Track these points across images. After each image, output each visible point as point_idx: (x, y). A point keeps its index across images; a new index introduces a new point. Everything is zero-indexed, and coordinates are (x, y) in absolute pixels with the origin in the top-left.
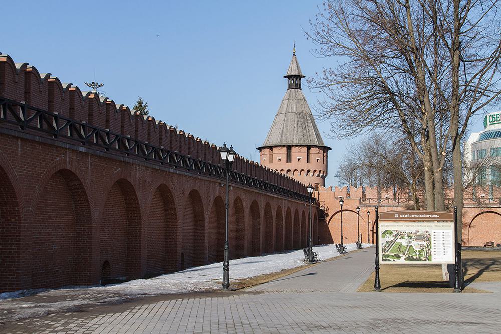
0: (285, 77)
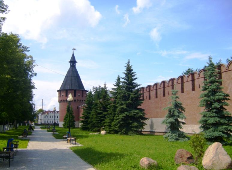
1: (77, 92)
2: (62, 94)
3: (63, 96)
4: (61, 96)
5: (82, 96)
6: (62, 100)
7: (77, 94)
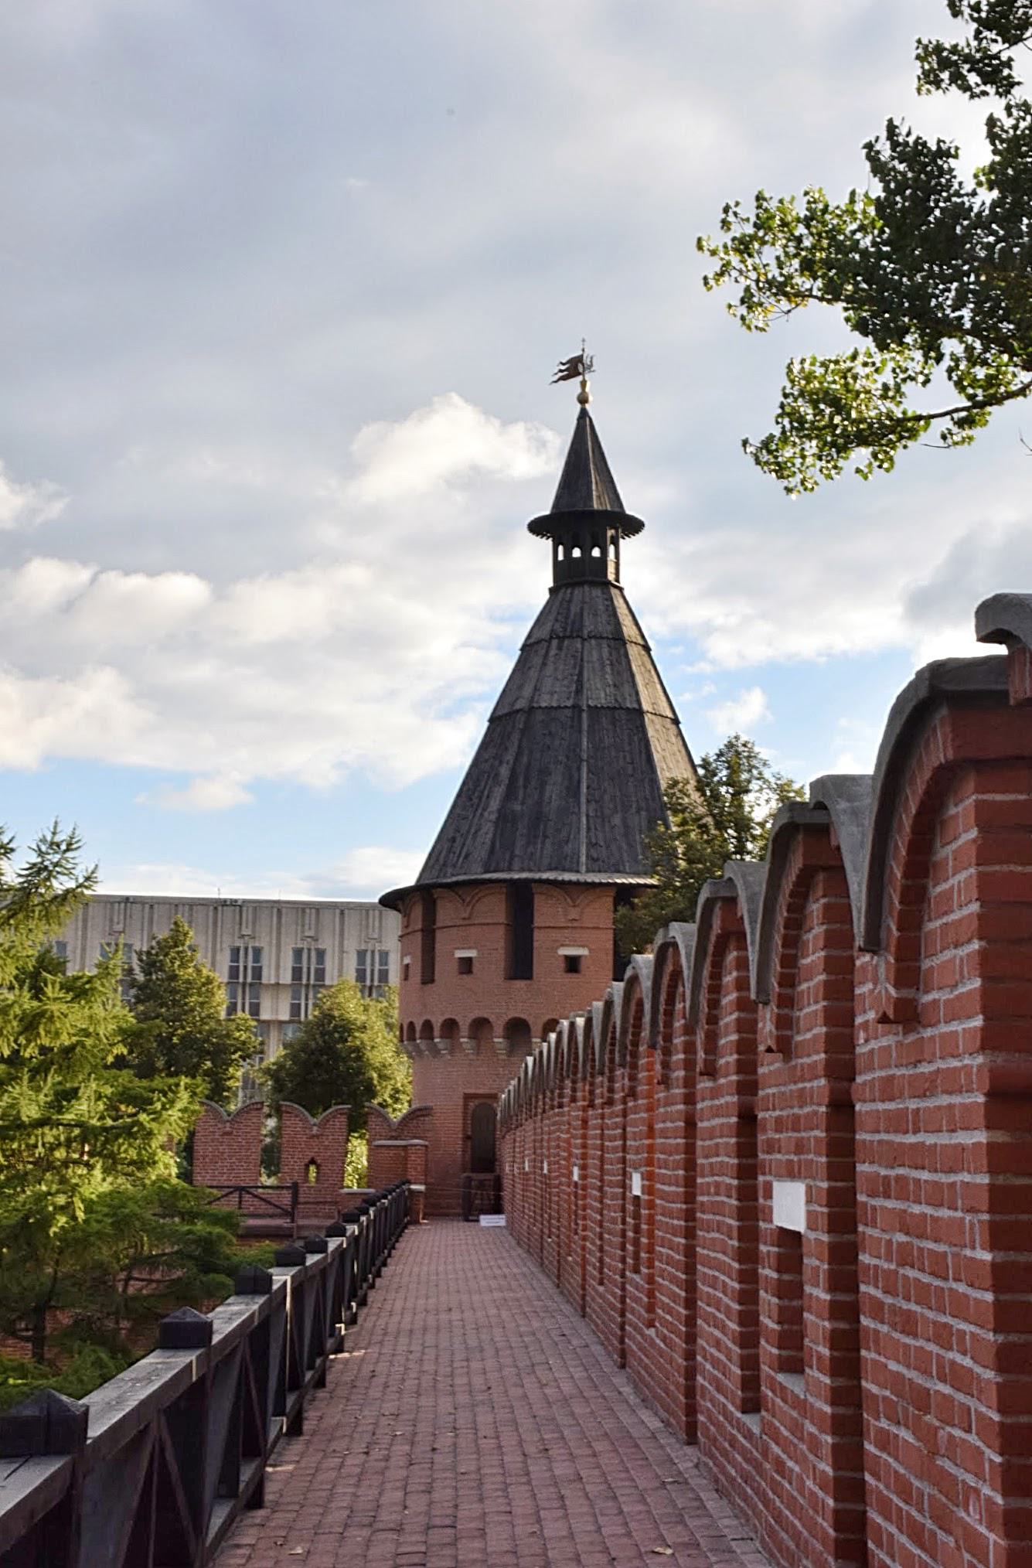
0: (538, 527)
1: (546, 911)
2: (454, 949)
4: (445, 968)
5: (520, 965)
6: (428, 1025)
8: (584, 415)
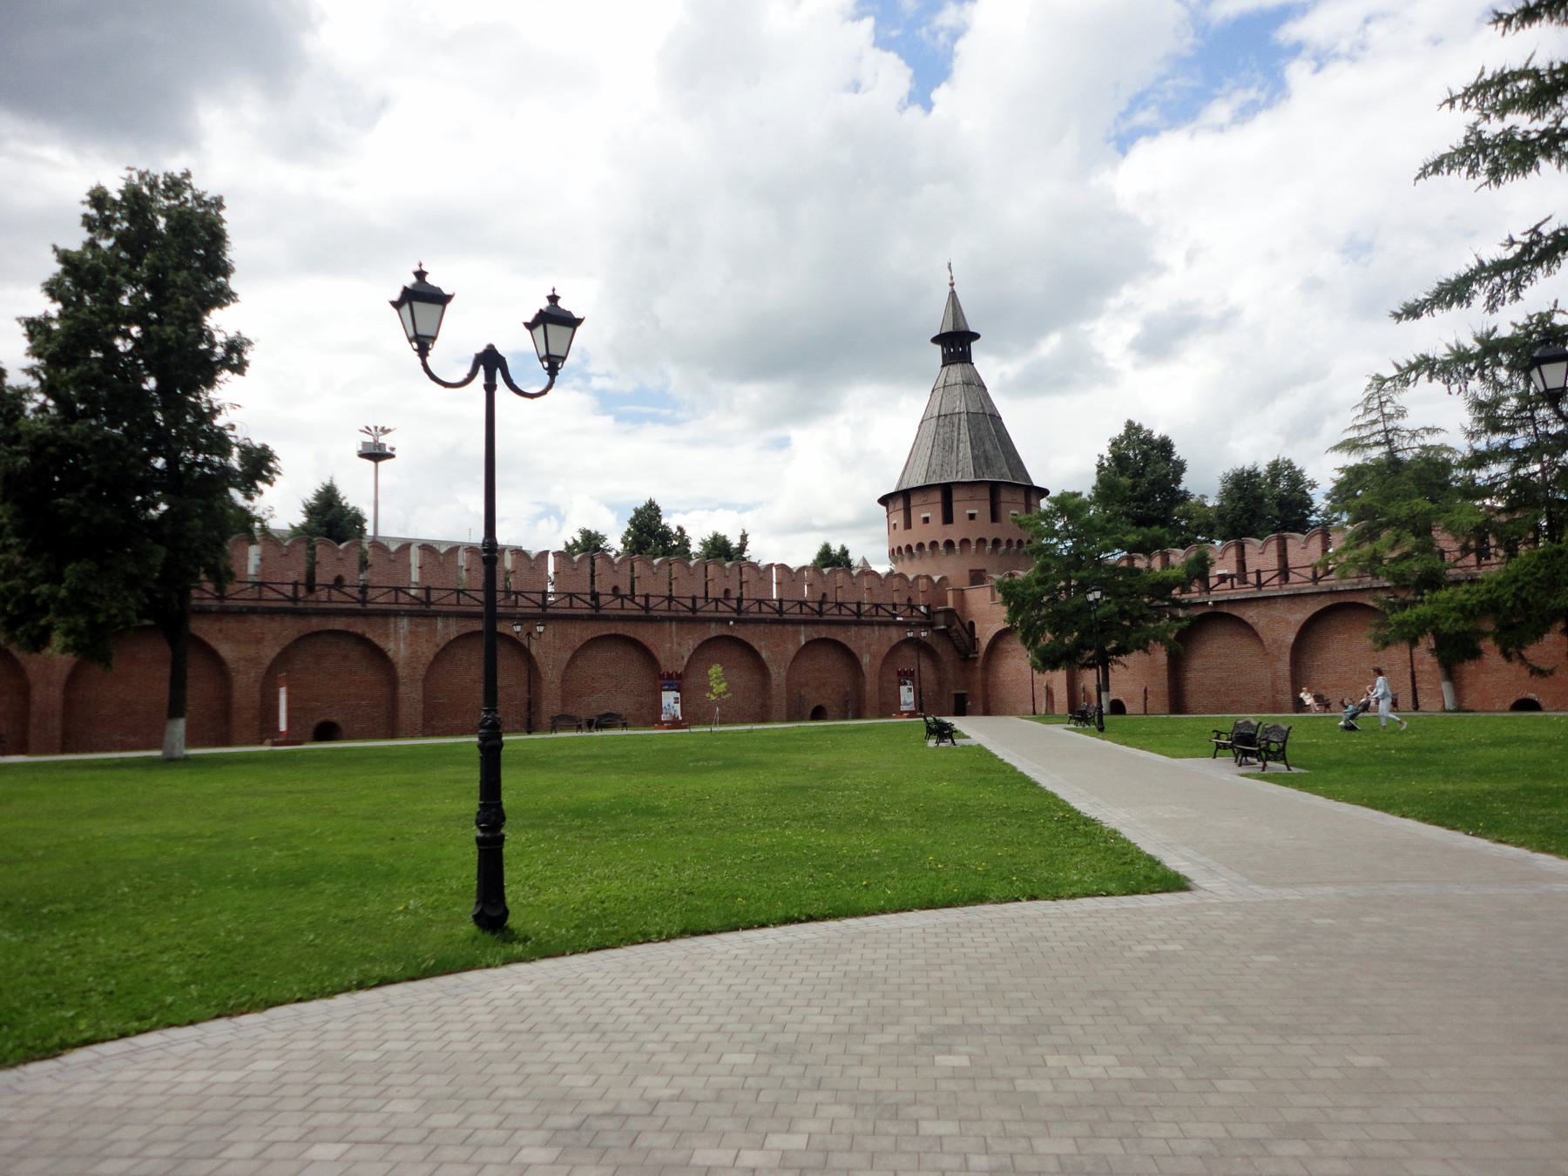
3: (926, 520)
7: (955, 506)
8: (953, 293)
